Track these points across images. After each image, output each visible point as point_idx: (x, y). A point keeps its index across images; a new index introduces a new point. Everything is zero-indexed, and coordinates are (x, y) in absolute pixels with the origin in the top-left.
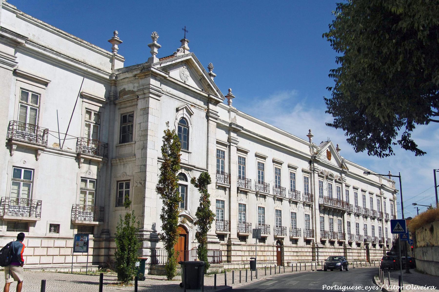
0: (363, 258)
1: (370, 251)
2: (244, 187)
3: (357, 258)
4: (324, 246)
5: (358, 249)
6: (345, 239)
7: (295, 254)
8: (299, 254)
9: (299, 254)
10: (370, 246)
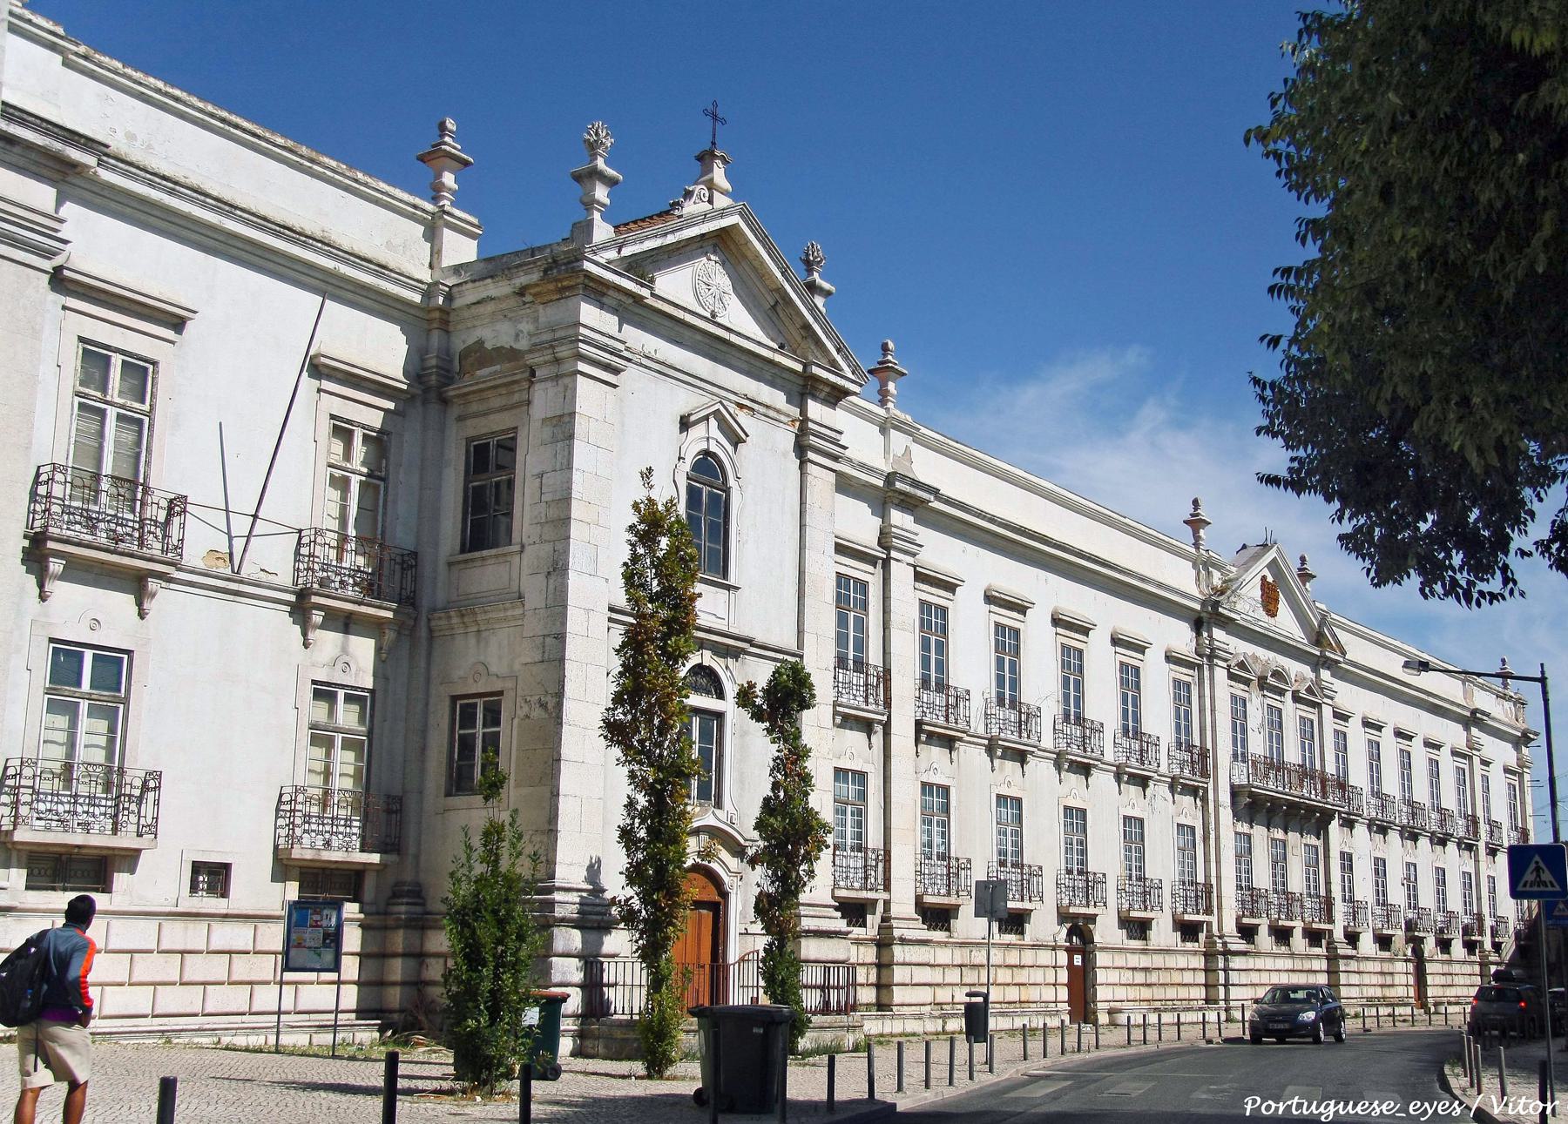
0: (1401, 992)
1: (1430, 968)
2: (942, 721)
3: (1378, 992)
4: (1251, 947)
5: (1383, 960)
6: (1331, 920)
7: (1140, 977)
8: (1153, 978)
9: (1153, 978)
10: (1430, 945)
